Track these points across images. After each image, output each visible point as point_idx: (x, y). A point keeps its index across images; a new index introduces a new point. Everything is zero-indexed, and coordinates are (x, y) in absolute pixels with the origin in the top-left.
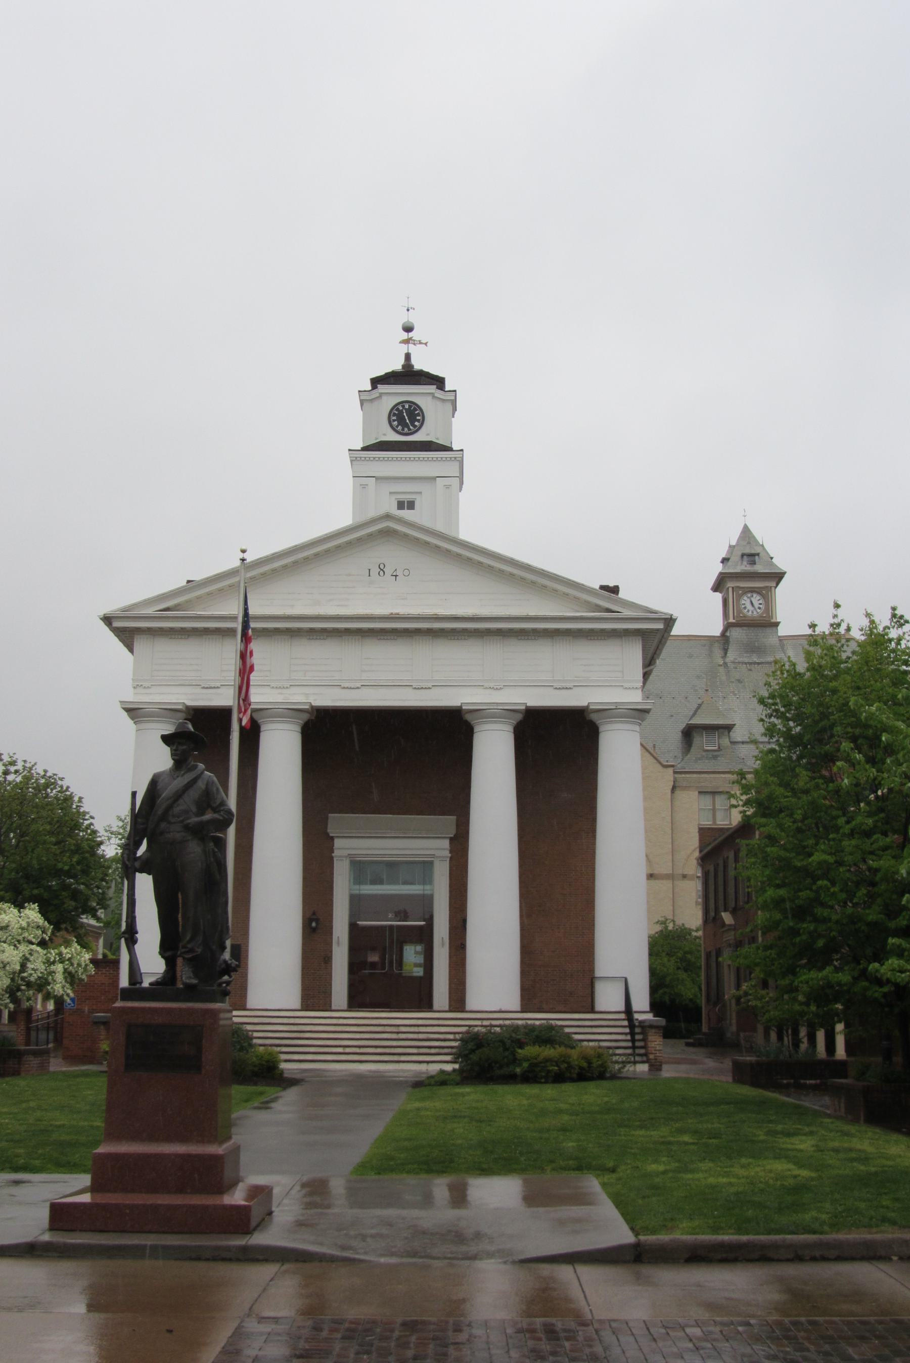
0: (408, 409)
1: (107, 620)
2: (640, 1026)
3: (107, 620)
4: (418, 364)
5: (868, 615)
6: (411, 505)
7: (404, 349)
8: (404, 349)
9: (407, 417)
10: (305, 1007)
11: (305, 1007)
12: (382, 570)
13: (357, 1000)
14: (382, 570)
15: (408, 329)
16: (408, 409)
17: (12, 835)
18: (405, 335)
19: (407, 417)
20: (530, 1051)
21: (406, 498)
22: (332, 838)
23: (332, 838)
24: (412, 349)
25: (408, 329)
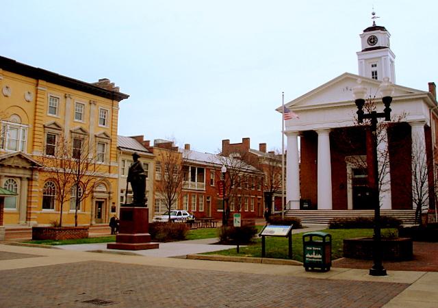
0: (374, 38)
1: (277, 110)
2: (165, 230)
3: (277, 110)
4: (378, 24)
5: (432, 85)
6: (376, 66)
7: (373, 20)
8: (373, 20)
9: (372, 40)
10: (393, 209)
11: (393, 209)
12: (347, 89)
13: (355, 208)
14: (347, 89)
15: (374, 14)
16: (374, 38)
17: (228, 238)
18: (373, 16)
19: (372, 40)
20: (9, 275)
21: (374, 64)
22: (110, 225)
23: (110, 225)
24: (375, 20)
25: (374, 14)
